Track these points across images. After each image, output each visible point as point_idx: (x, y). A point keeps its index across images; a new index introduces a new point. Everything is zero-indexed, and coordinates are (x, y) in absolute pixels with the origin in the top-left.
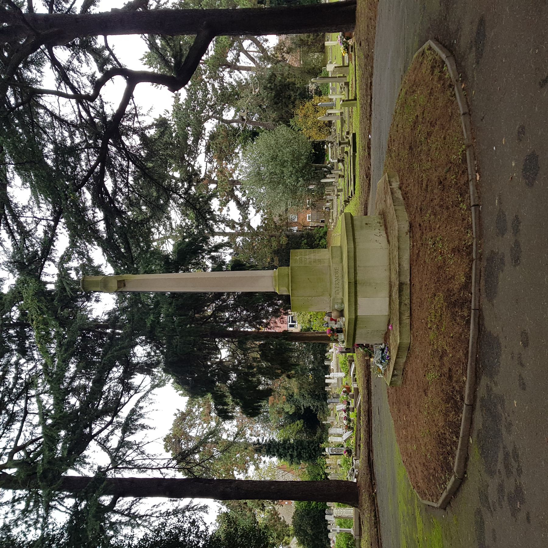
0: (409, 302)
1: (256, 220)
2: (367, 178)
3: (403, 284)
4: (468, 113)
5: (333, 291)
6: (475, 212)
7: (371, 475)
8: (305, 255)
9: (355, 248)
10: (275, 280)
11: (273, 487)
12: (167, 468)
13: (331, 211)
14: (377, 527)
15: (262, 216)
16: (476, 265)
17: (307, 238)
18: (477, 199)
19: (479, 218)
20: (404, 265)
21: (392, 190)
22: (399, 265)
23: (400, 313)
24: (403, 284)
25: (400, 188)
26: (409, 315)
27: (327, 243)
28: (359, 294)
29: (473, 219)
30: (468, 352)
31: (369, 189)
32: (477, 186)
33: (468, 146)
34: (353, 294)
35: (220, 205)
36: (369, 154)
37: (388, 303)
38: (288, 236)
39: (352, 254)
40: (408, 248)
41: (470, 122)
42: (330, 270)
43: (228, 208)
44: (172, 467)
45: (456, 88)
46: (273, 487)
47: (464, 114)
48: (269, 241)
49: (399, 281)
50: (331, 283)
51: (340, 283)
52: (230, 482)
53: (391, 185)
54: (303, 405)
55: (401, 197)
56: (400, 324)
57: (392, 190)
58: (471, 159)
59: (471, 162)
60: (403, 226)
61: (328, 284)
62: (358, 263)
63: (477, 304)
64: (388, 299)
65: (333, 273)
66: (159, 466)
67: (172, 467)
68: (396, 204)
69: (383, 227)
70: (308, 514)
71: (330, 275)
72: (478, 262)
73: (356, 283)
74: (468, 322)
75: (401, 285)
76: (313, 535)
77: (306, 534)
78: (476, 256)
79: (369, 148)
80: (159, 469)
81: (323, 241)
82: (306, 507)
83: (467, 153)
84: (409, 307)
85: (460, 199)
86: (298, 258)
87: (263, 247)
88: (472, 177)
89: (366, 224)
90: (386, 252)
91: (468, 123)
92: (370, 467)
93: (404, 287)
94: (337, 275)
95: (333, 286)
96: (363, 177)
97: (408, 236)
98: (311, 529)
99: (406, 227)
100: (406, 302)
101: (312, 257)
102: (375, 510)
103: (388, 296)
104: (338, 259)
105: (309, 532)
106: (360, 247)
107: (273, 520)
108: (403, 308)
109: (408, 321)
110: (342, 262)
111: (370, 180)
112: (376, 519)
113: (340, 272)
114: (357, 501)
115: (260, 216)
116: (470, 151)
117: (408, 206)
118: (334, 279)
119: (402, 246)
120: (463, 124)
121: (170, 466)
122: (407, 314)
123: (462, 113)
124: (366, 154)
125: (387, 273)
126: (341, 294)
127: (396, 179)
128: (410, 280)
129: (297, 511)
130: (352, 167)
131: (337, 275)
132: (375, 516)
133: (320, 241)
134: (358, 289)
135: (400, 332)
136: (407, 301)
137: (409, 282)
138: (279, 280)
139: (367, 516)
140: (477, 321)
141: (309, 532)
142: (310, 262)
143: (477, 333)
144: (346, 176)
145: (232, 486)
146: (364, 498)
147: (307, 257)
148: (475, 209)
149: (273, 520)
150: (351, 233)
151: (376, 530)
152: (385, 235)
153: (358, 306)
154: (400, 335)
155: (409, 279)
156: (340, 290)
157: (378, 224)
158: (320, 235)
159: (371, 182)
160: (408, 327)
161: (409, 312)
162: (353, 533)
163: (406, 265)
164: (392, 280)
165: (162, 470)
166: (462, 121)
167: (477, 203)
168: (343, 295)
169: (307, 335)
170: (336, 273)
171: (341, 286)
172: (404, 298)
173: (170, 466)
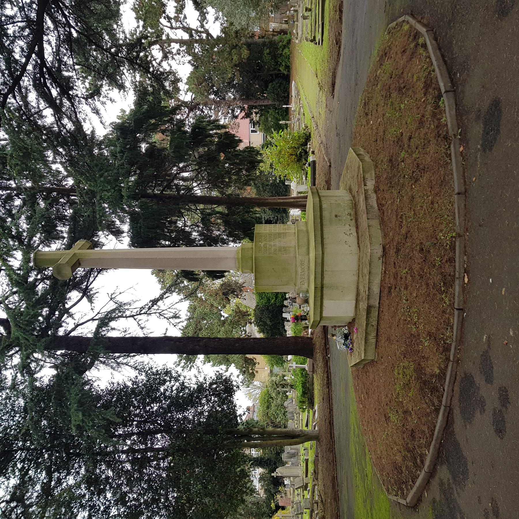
0: (376, 323)
1: (215, 29)
2: (337, 44)
3: (372, 307)
4: (464, 193)
5: (299, 281)
6: (459, 317)
7: (325, 340)
8: (270, 241)
9: (323, 253)
10: (239, 263)
11: (237, 345)
12: (140, 314)
13: (296, 23)
14: (328, 387)
15: (221, 25)
16: (452, 367)
17: (270, 48)
18: (462, 302)
19: (462, 322)
20: (374, 289)
21: (366, 191)
22: (369, 289)
23: (366, 333)
24: (372, 307)
25: (376, 192)
26: (375, 335)
27: (291, 53)
28: (325, 297)
29: (455, 321)
30: (433, 434)
31: (338, 58)
32: (463, 288)
33: (459, 235)
34: (319, 299)
35: (176, 13)
36: (340, 18)
37: (354, 306)
38: (248, 45)
39: (320, 261)
40: (380, 273)
41: (465, 205)
42: (296, 261)
43: (185, 15)
44: (144, 313)
45: (452, 146)
46: (237, 345)
47: (459, 194)
48: (230, 54)
49: (368, 304)
50: (296, 272)
51: (306, 275)
52: (199, 340)
53: (365, 185)
54: (265, 218)
55: (375, 205)
56: (366, 343)
57: (366, 191)
58: (460, 254)
59: (460, 257)
60: (376, 251)
61: (294, 274)
62: (326, 268)
63: (449, 402)
64: (354, 302)
65: (298, 263)
66: (133, 314)
67: (144, 313)
68: (370, 216)
69: (354, 221)
70: (268, 309)
71: (296, 265)
72: (455, 365)
73: (322, 287)
74: (437, 411)
75: (369, 308)
76: (272, 325)
77: (265, 324)
78: (454, 359)
79: (341, 11)
80: (133, 316)
81: (286, 50)
82: (266, 303)
83: (457, 244)
84: (376, 328)
85: (443, 289)
87: (223, 60)
88: (459, 275)
89: (336, 216)
90: (355, 258)
91: (463, 206)
92: (325, 333)
93: (373, 309)
94: (302, 267)
95: (299, 277)
96: (333, 41)
97: (381, 261)
98: (270, 321)
99: (379, 251)
100: (373, 324)
101: (277, 243)
102: (327, 372)
103: (355, 299)
104: (304, 249)
105: (268, 322)
106: (326, 251)
107: (237, 318)
108: (370, 328)
109: (374, 341)
110: (308, 254)
111: (340, 47)
112: (328, 380)
113: (306, 264)
114: (312, 355)
115: (219, 24)
116: (460, 242)
117: (383, 223)
118: (299, 270)
119: (373, 271)
120: (456, 204)
121: (142, 312)
122: (374, 334)
123: (456, 191)
124: (338, 17)
125: (356, 278)
126: (306, 285)
127: (371, 174)
128: (379, 303)
129: (257, 306)
130: (320, 7)
131: (302, 267)
132: (328, 377)
133: (283, 51)
134: (324, 292)
135: (365, 350)
136: (375, 323)
137: (378, 305)
138: (242, 263)
139: (320, 363)
140: (446, 414)
141: (268, 322)
142: (275, 250)
143: (445, 423)
144: (313, 10)
145: (201, 344)
146: (319, 355)
147: (272, 243)
148: (459, 314)
149: (237, 318)
151: (328, 390)
152: (355, 234)
153: (324, 307)
154: (365, 353)
155: (378, 302)
156: (306, 281)
157: (349, 217)
158: (284, 43)
159: (342, 51)
160: (374, 346)
161: (375, 332)
162: (307, 369)
163: (376, 289)
164: (361, 287)
165: (136, 317)
166: (456, 201)
167: (461, 307)
168: (309, 286)
169: (270, 201)
170: (302, 264)
171: (306, 277)
172: (371, 320)
173: (142, 312)
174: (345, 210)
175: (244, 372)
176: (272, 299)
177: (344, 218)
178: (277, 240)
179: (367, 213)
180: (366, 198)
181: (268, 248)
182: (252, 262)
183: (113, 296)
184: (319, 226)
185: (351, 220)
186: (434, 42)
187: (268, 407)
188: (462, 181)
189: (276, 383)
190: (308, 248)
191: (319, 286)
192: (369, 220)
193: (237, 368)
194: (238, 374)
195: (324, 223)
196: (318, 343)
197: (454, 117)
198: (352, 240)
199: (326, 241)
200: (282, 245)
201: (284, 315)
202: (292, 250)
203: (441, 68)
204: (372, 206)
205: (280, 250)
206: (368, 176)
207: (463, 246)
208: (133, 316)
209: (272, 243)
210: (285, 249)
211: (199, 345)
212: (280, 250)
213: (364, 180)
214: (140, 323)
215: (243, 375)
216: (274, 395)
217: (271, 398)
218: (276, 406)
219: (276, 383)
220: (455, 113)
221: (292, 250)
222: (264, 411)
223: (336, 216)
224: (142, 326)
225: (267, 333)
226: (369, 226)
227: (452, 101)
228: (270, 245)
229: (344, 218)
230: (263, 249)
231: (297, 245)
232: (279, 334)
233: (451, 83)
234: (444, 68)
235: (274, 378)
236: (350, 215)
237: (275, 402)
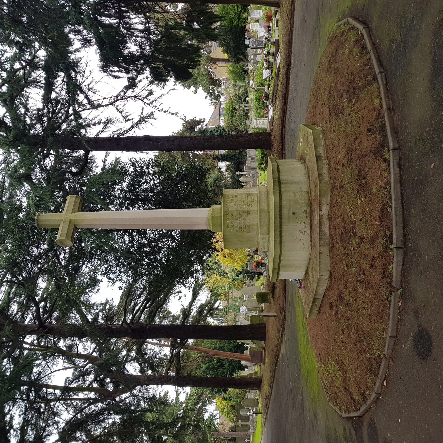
7: (282, 146)
8: (236, 219)
11: (206, 144)
22: (316, 292)
46: (206, 144)
53: (320, 211)
55: (327, 232)
67: (121, 99)
69: (309, 219)
80: (112, 104)
82: (229, 24)
86: (230, 222)
92: (282, 139)
98: (234, 43)
99: (327, 276)
104: (265, 229)
105: (232, 44)
110: (268, 233)
127: (327, 198)
147: (238, 221)
150: (279, 233)
152: (309, 232)
157: (305, 214)
174: (301, 207)
175: (211, 94)
176: (235, 20)
177: (301, 216)
178: (242, 218)
179: (320, 240)
180: (320, 224)
181: (234, 227)
182: (221, 227)
183: (91, 86)
184: (279, 226)
185: (307, 217)
186: (397, 169)
187: (232, 117)
188: (395, 328)
189: (239, 96)
190: (269, 228)
191: (277, 267)
192: (321, 247)
193: (205, 92)
194: (206, 95)
195: (283, 221)
196: (276, 135)
197: (400, 274)
198: (306, 238)
199: (284, 239)
200: (247, 223)
201: (247, 42)
202: (255, 228)
203: (398, 212)
204: (324, 233)
205: (245, 228)
206: (324, 200)
207: (387, 364)
208: (112, 104)
209: (238, 221)
210: (248, 227)
211: (174, 144)
212: (245, 228)
213: (320, 205)
214: (118, 108)
215: (210, 97)
216: (237, 107)
217: (235, 109)
218: (239, 116)
219: (239, 96)
220: (401, 269)
221: (255, 228)
222: (228, 120)
223: (294, 214)
224: (121, 110)
225: (231, 54)
226: (320, 253)
227: (401, 258)
228: (236, 223)
229: (301, 216)
230: (230, 227)
231: (259, 223)
232: (242, 54)
233: (404, 238)
234: (400, 213)
235: (237, 92)
236: (306, 212)
237: (238, 113)
